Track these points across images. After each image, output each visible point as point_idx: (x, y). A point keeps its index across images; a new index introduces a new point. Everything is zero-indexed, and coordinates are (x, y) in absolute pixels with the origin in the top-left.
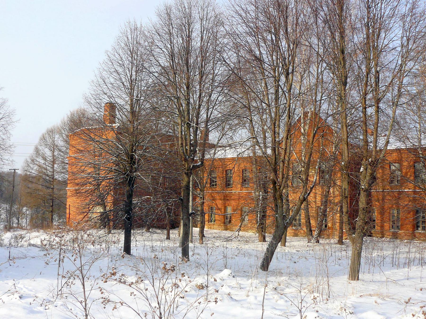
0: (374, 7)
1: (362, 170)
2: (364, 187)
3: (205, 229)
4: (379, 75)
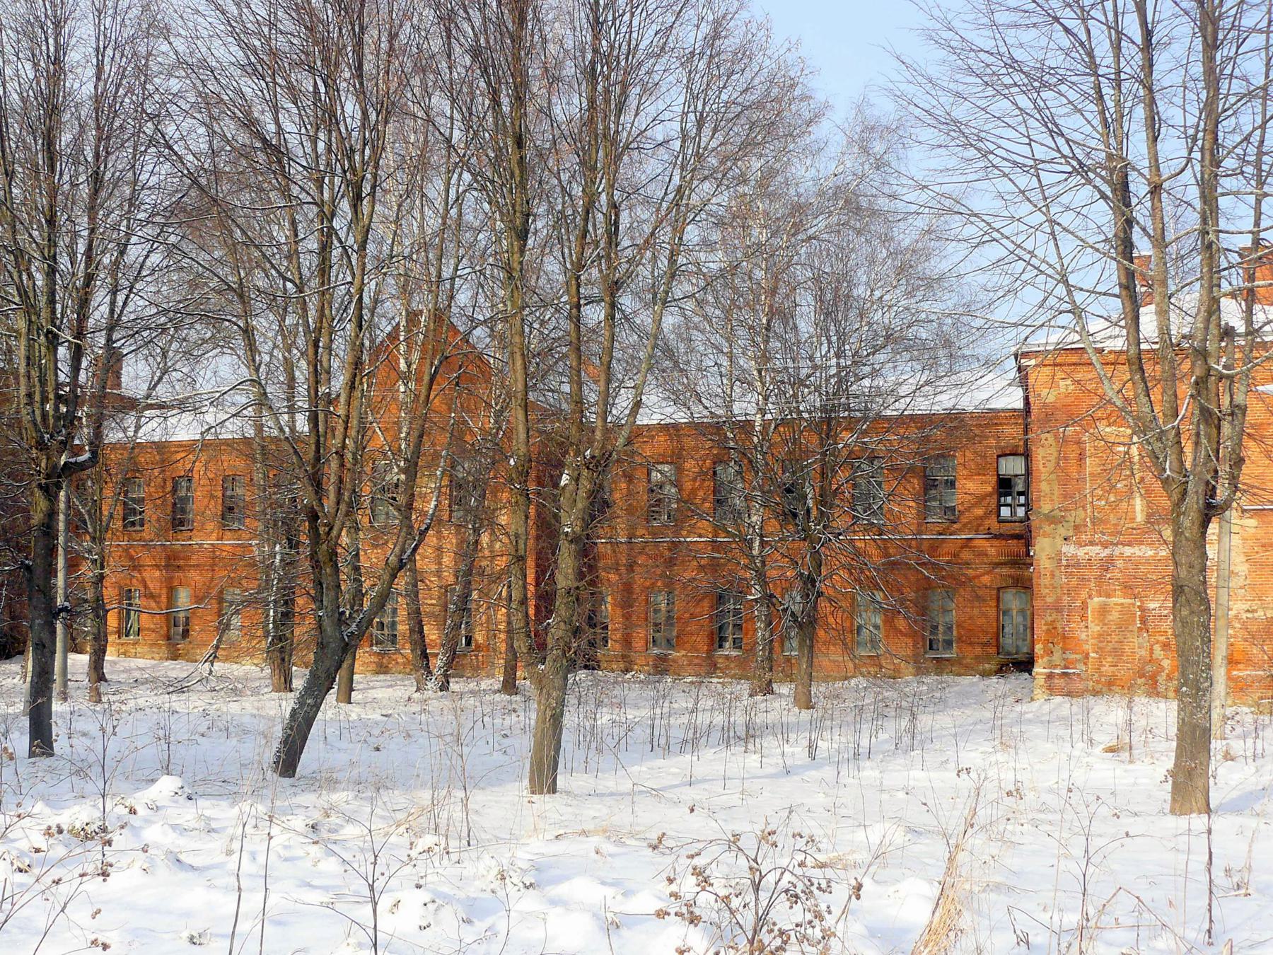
0: (610, 23)
1: (565, 480)
3: (106, 658)
4: (617, 215)
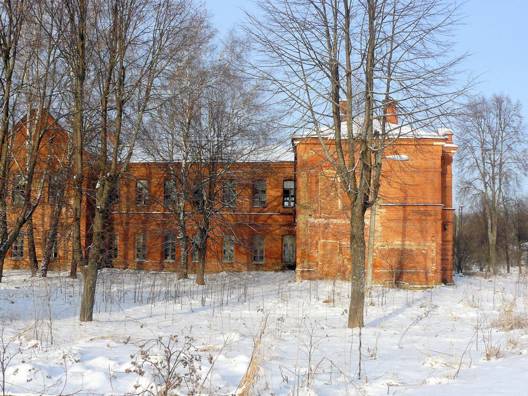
2: (99, 207)
